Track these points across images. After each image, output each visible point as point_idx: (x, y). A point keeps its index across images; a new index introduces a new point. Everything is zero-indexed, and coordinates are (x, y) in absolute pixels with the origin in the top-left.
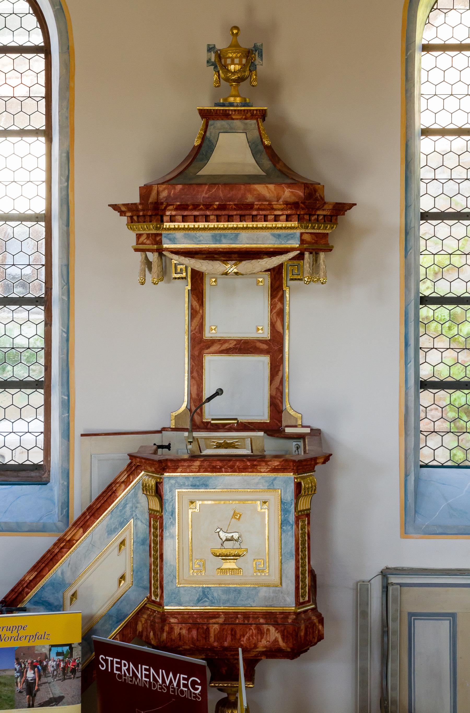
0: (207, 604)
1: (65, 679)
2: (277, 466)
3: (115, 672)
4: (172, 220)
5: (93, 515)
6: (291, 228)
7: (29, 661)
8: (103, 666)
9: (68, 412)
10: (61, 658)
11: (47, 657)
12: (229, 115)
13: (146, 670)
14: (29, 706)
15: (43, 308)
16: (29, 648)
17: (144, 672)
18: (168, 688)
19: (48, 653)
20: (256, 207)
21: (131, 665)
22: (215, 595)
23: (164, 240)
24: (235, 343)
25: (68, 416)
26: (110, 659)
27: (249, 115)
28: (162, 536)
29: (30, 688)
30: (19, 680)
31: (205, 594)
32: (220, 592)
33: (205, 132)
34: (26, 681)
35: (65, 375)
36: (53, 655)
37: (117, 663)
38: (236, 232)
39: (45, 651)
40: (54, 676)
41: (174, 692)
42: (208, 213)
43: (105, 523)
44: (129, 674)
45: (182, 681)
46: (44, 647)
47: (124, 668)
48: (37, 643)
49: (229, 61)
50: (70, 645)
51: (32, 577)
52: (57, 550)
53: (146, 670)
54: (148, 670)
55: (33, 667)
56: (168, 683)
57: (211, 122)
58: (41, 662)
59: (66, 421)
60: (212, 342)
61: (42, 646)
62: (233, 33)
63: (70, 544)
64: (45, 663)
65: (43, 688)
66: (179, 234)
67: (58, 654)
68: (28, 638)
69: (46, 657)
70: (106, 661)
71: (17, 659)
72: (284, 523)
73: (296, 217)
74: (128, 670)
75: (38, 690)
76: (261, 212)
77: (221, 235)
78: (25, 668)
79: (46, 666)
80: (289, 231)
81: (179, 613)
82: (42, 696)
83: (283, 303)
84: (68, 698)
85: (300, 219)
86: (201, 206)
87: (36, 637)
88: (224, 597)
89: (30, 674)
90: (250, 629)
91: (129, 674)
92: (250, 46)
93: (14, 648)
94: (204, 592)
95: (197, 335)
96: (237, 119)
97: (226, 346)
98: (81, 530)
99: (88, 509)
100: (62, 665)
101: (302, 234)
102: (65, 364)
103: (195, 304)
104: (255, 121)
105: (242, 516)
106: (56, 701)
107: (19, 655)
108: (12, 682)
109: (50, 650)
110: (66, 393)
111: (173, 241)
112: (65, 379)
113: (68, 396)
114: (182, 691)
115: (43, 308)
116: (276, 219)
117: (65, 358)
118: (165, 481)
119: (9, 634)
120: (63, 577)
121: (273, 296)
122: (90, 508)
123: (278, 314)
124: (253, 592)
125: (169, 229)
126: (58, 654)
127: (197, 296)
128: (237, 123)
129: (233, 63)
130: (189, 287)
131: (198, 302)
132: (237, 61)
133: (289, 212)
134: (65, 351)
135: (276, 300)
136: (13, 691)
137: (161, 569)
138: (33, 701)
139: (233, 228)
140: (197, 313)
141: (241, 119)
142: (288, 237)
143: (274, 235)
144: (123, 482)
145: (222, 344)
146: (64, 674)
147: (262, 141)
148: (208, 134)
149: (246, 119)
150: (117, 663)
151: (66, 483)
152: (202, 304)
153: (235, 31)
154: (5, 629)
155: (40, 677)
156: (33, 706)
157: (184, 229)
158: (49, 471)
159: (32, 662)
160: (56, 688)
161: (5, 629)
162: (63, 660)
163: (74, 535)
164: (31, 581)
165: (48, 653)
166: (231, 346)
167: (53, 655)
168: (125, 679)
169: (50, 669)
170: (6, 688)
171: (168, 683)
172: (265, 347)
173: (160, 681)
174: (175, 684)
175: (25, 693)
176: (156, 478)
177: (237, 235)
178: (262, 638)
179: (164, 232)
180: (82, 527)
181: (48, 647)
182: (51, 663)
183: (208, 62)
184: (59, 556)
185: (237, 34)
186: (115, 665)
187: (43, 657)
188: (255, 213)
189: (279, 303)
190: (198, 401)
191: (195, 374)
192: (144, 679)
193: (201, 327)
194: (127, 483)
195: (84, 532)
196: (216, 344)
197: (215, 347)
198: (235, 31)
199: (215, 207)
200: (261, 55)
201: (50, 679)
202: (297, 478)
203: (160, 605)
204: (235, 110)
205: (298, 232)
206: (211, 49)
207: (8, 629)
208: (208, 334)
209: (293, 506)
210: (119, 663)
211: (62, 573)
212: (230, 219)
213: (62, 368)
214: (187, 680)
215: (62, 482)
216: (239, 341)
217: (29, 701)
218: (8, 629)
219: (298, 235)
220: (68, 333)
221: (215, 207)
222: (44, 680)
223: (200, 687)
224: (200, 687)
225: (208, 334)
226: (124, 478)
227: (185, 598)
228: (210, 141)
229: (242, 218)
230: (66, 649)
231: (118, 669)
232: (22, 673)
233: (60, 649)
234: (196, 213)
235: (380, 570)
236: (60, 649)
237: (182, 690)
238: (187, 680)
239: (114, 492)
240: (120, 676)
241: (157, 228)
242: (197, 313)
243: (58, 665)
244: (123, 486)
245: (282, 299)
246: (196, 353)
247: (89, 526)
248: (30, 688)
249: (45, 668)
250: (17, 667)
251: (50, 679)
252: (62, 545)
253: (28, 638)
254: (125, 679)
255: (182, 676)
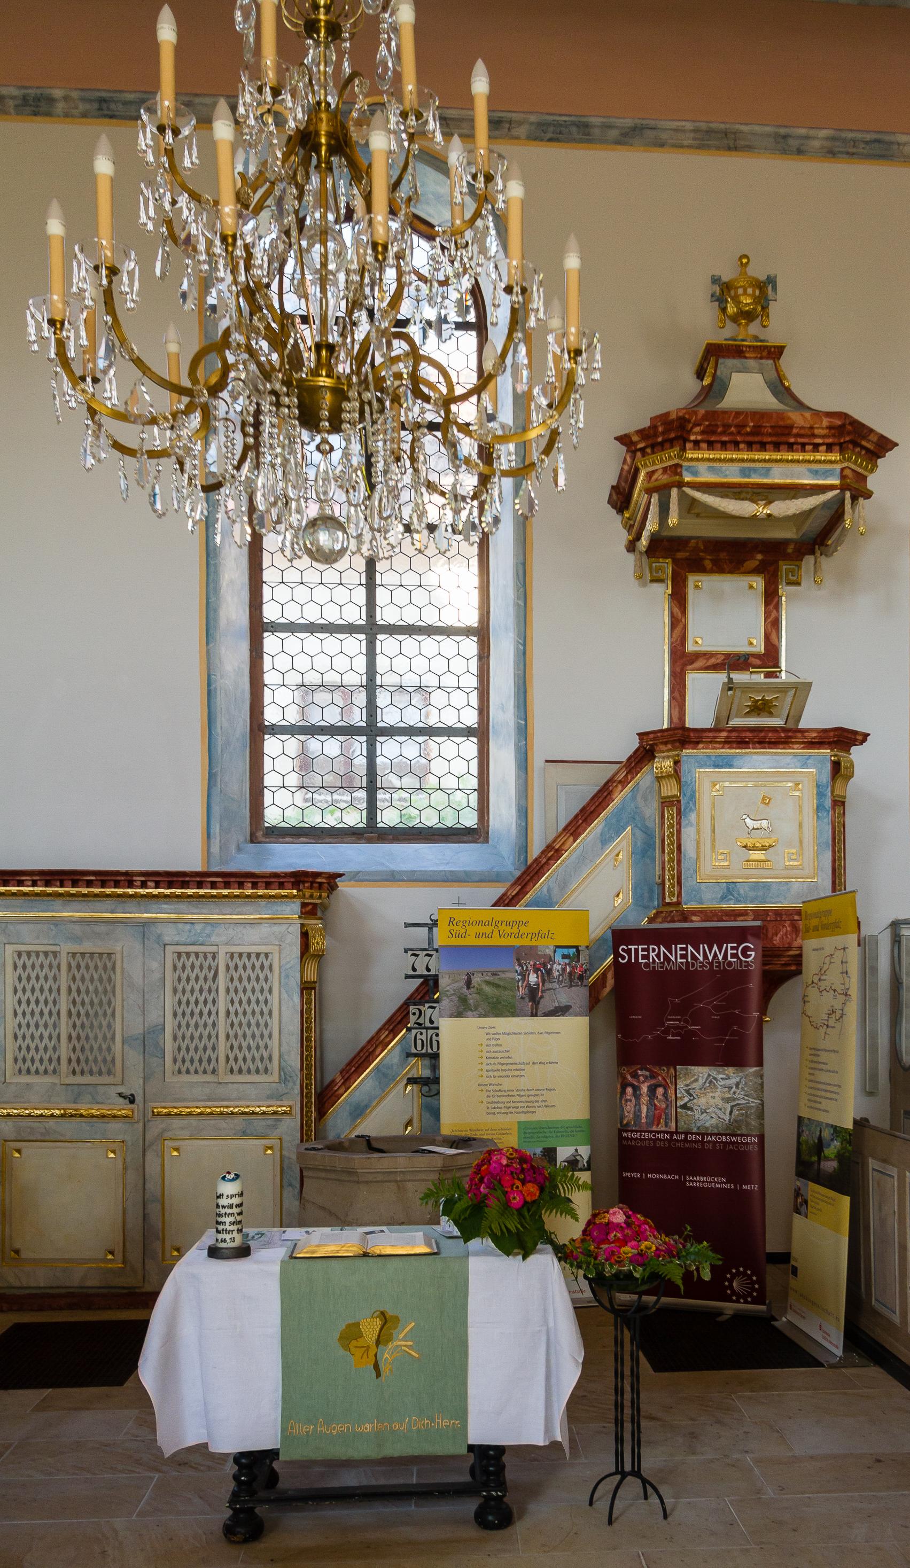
0: (732, 902)
1: (571, 986)
2: (814, 738)
3: (640, 961)
4: (697, 444)
5: (585, 821)
6: (831, 462)
7: (532, 963)
8: (623, 958)
9: (526, 740)
10: (567, 961)
11: (551, 960)
12: (742, 352)
13: (682, 949)
14: (532, 1016)
15: (475, 639)
16: (531, 947)
17: (679, 952)
18: (711, 964)
19: (552, 955)
20: (795, 431)
21: (662, 948)
22: (742, 892)
23: (684, 473)
24: (723, 657)
25: (526, 744)
26: (633, 947)
27: (765, 354)
28: (679, 823)
29: (533, 994)
30: (520, 984)
31: (730, 889)
32: (747, 889)
33: (715, 371)
34: (529, 985)
35: (522, 696)
36: (558, 958)
37: (643, 950)
38: (768, 465)
39: (549, 952)
40: (560, 982)
41: (719, 967)
42: (739, 439)
43: (599, 830)
44: (659, 959)
45: (730, 952)
46: (547, 947)
47: (652, 954)
48: (540, 943)
49: (740, 291)
50: (577, 947)
51: (515, 892)
52: (544, 860)
53: (682, 949)
54: (686, 949)
55: (536, 970)
56: (710, 958)
57: (720, 361)
58: (545, 965)
59: (523, 750)
60: (697, 656)
61: (546, 946)
62: (742, 263)
63: (558, 853)
64: (549, 967)
65: (547, 994)
66: (702, 467)
67: (564, 957)
68: (530, 936)
69: (551, 960)
70: (628, 952)
71: (518, 960)
72: (819, 808)
73: (837, 448)
74: (658, 956)
75: (542, 997)
76: (800, 440)
77: (750, 469)
78: (527, 970)
79: (551, 970)
80: (828, 467)
81: (701, 912)
82: (547, 1003)
83: (778, 611)
84: (575, 1008)
85: (842, 451)
86: (733, 429)
87: (538, 935)
88: (752, 894)
89: (533, 978)
90: (784, 926)
91: (659, 959)
92: (763, 278)
93: (514, 946)
94: (728, 889)
95: (679, 648)
96: (750, 358)
97: (713, 661)
98: (571, 839)
99: (581, 811)
100: (568, 969)
101: (842, 470)
102: (521, 682)
103: (677, 611)
104: (771, 362)
105: (772, 801)
106: (561, 1011)
107: (521, 954)
108: (511, 986)
109: (555, 951)
110: (523, 716)
111: (695, 473)
112: (522, 700)
113: (526, 721)
114: (730, 964)
115: (475, 639)
116: (816, 447)
117: (522, 675)
118: (683, 759)
119: (508, 930)
120: (550, 895)
121: (767, 604)
122: (583, 810)
123: (773, 624)
124: (785, 888)
125: (692, 460)
126: (564, 957)
127: (679, 602)
128: (752, 363)
129: (745, 293)
130: (669, 591)
131: (680, 609)
132: (750, 291)
133: (831, 440)
134: (522, 666)
135: (771, 607)
136: (514, 996)
137: (679, 862)
138: (537, 1009)
139: (765, 461)
140: (678, 623)
141: (756, 358)
142: (826, 474)
143: (810, 471)
144: (620, 782)
145: (708, 659)
146: (571, 980)
147: (781, 381)
148: (718, 373)
149: (761, 358)
150: (643, 950)
151: (523, 824)
152: (684, 611)
153: (744, 261)
154: (504, 924)
155: (544, 981)
156: (536, 1016)
157: (709, 460)
158: (488, 833)
159: (535, 965)
160: (563, 995)
161: (504, 924)
162: (569, 964)
163: (563, 844)
164: (513, 897)
165: (552, 955)
166: (719, 661)
167: (558, 958)
168: (654, 967)
169: (556, 974)
170: (506, 993)
171: (710, 958)
172: (758, 662)
173: (701, 958)
174: (720, 958)
175: (527, 1000)
176: (672, 757)
177: (769, 470)
178: (797, 936)
179: (685, 464)
180: (572, 834)
181: (552, 948)
182: (556, 967)
183: (712, 296)
184: (546, 869)
185: (747, 263)
186: (641, 953)
187: (547, 960)
188: (792, 440)
189: (775, 611)
190: (771, 598)
191: (677, 694)
192: (679, 960)
193: (683, 638)
194: (624, 783)
195: (575, 841)
196: (701, 659)
197: (700, 663)
198: (744, 261)
199: (748, 429)
200: (775, 289)
201: (555, 985)
202: (835, 756)
203: (678, 903)
204: (750, 347)
205: (838, 467)
206: (715, 280)
207: (508, 924)
208: (690, 647)
209: (829, 789)
210: (647, 950)
211: (549, 890)
212: (763, 447)
213: (519, 689)
214: (736, 948)
215: (519, 822)
216: (728, 655)
217: (532, 1009)
218: (508, 924)
219: (838, 471)
220: (524, 645)
221: (748, 429)
222: (548, 985)
223: (753, 953)
224: (753, 953)
225: (690, 647)
226: (621, 776)
227: (707, 896)
228: (722, 380)
229: (777, 447)
230: (572, 951)
231: (644, 957)
232: (524, 976)
233: (566, 951)
234: (725, 439)
235: (889, 922)
236: (566, 951)
237: (730, 962)
238: (736, 948)
239: (610, 793)
240: (647, 965)
241: (680, 457)
242: (678, 623)
243: (564, 970)
244: (620, 787)
245: (777, 607)
246: (678, 669)
247: (580, 834)
248: (533, 994)
249: (549, 972)
250: (519, 969)
251: (555, 985)
252: (550, 855)
253: (530, 936)
254: (654, 967)
255: (729, 945)
